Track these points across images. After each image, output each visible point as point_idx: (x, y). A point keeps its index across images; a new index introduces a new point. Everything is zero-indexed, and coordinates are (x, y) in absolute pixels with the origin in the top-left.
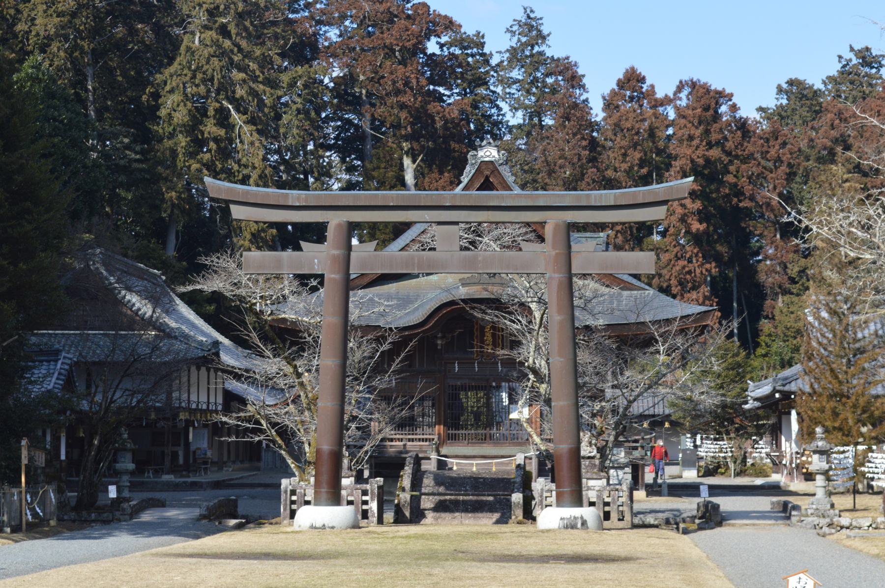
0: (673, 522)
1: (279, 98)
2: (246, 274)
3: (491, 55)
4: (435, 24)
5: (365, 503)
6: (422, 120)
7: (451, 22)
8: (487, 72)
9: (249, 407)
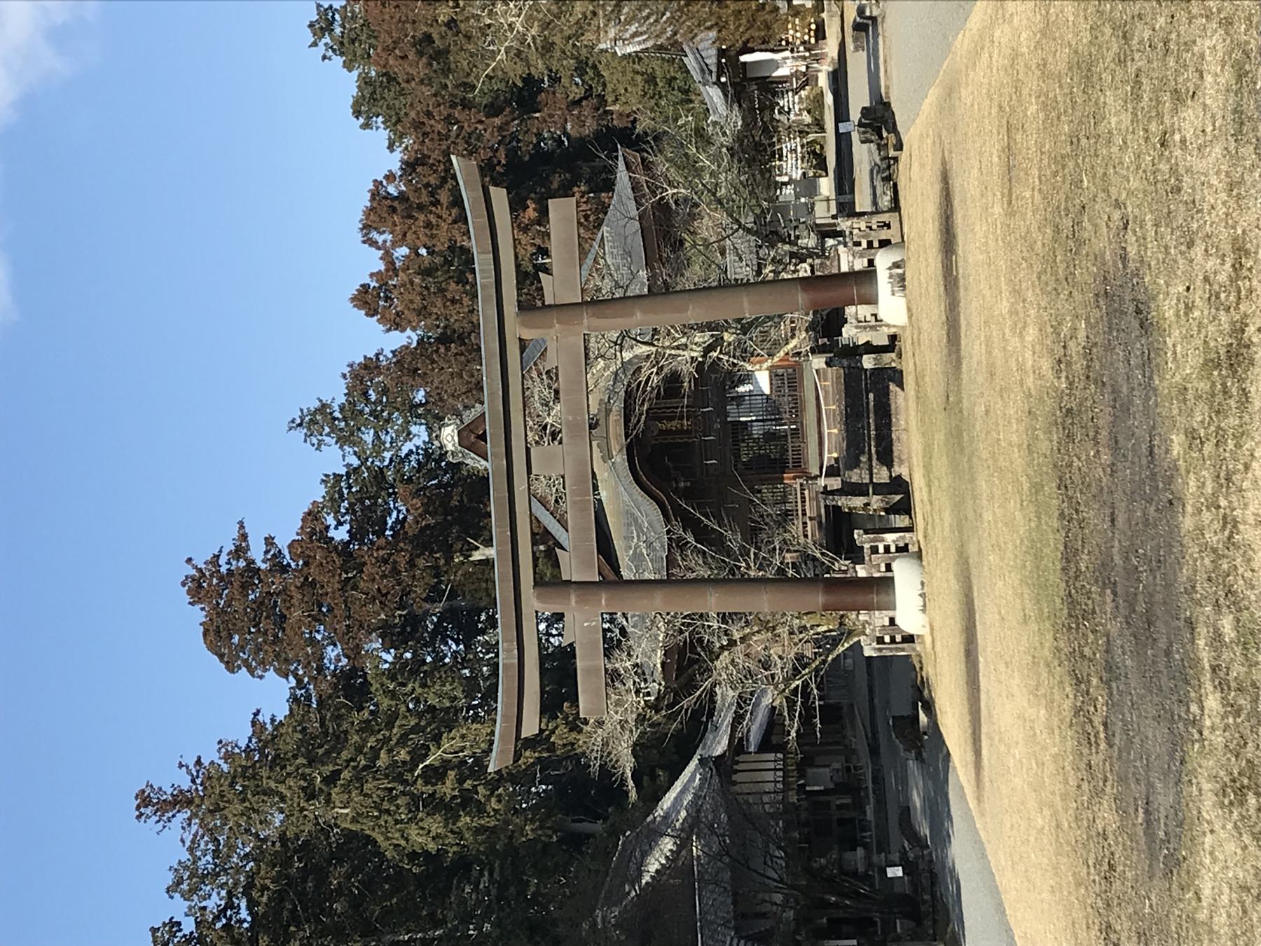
0: (887, 172)
1: (409, 710)
2: (611, 724)
3: (348, 465)
4: (313, 532)
5: (887, 549)
6: (425, 541)
7: (309, 513)
8: (368, 468)
9: (776, 703)
